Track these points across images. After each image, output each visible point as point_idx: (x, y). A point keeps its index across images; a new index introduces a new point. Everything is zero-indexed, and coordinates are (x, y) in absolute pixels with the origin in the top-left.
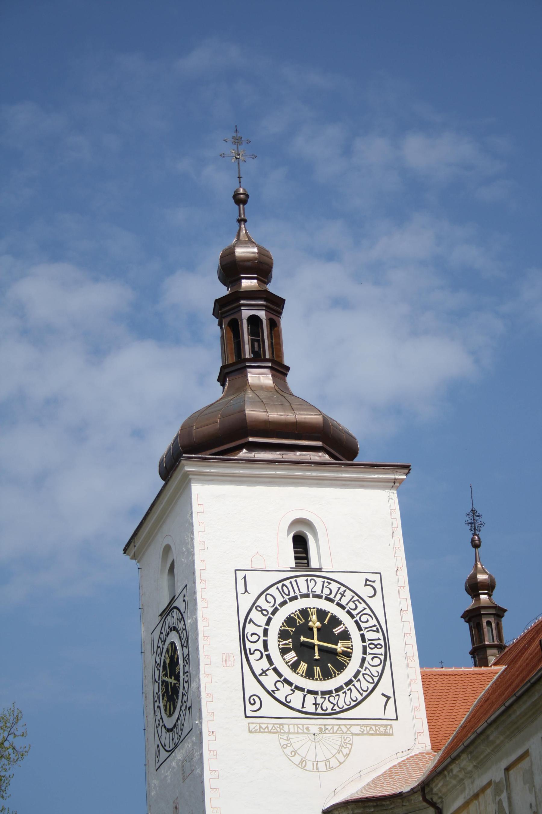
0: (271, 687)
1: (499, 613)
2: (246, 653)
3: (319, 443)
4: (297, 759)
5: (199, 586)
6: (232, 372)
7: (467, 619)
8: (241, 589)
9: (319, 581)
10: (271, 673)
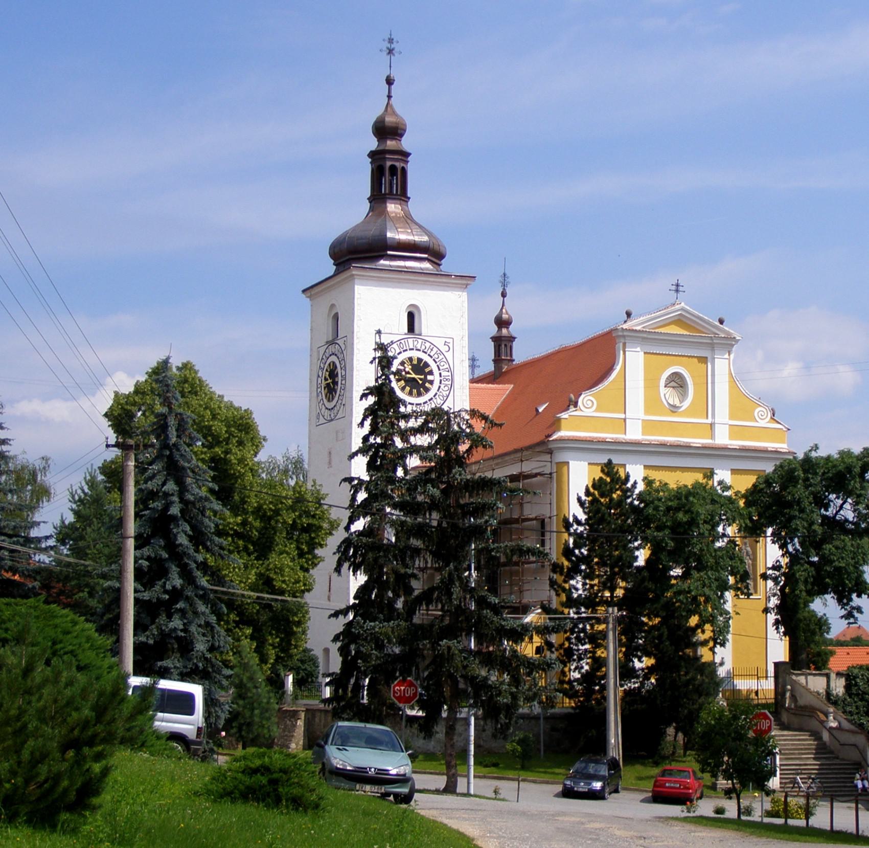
1: (512, 339)
3: (426, 256)
5: (356, 341)
6: (378, 198)
7: (628, 699)
9: (420, 341)
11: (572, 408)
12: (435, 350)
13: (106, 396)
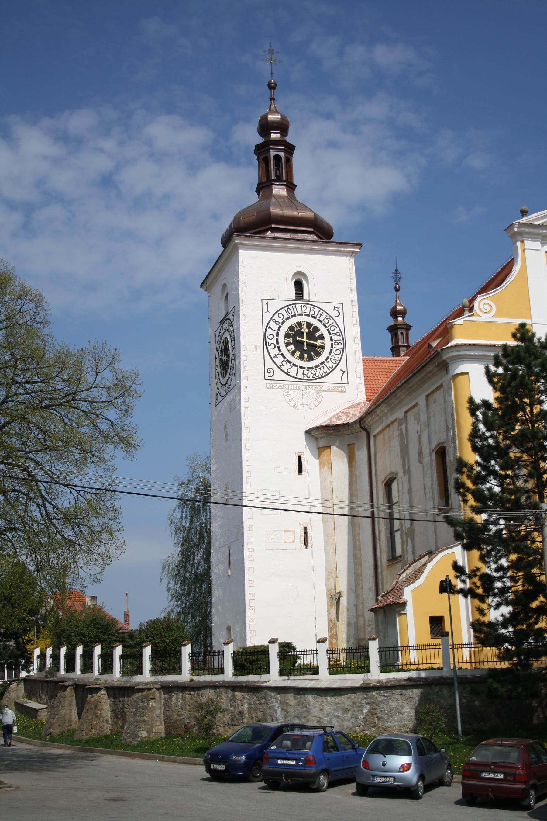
0: (279, 364)
1: (408, 328)
2: (266, 345)
3: (311, 229)
4: (292, 403)
6: (264, 187)
8: (265, 309)
9: (308, 306)
10: (280, 356)
11: (467, 313)
12: (324, 315)
13: (58, 383)
